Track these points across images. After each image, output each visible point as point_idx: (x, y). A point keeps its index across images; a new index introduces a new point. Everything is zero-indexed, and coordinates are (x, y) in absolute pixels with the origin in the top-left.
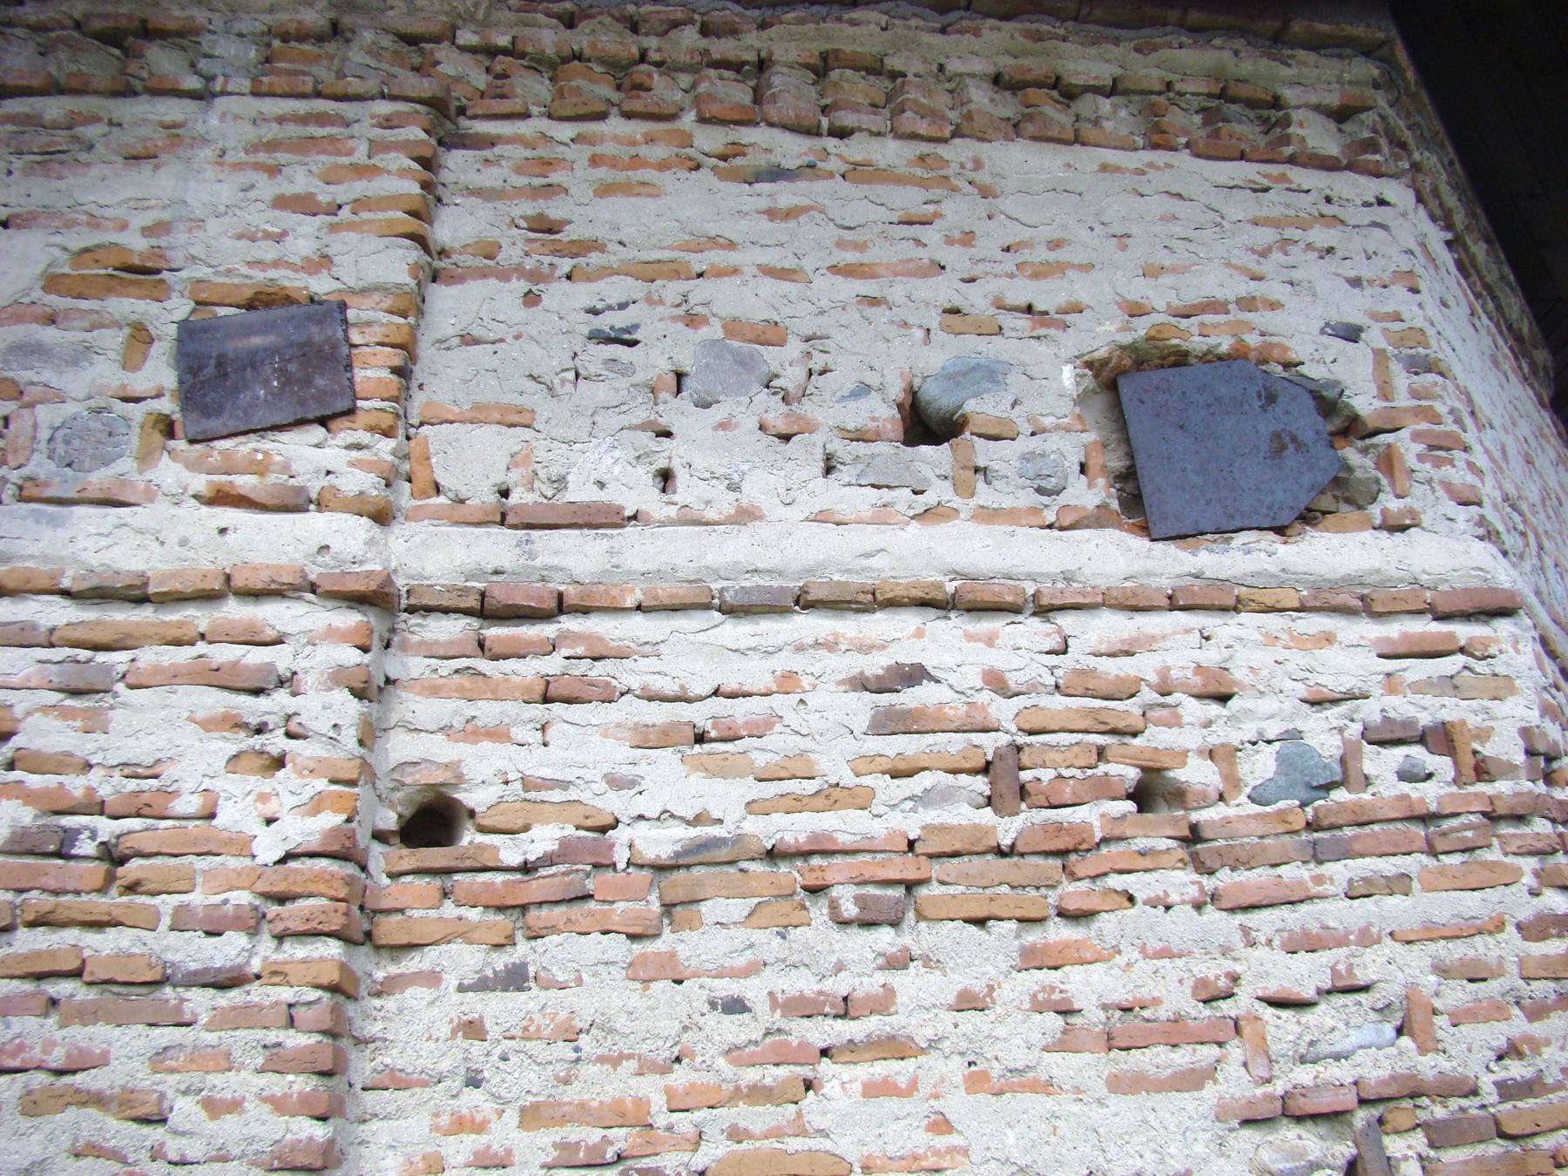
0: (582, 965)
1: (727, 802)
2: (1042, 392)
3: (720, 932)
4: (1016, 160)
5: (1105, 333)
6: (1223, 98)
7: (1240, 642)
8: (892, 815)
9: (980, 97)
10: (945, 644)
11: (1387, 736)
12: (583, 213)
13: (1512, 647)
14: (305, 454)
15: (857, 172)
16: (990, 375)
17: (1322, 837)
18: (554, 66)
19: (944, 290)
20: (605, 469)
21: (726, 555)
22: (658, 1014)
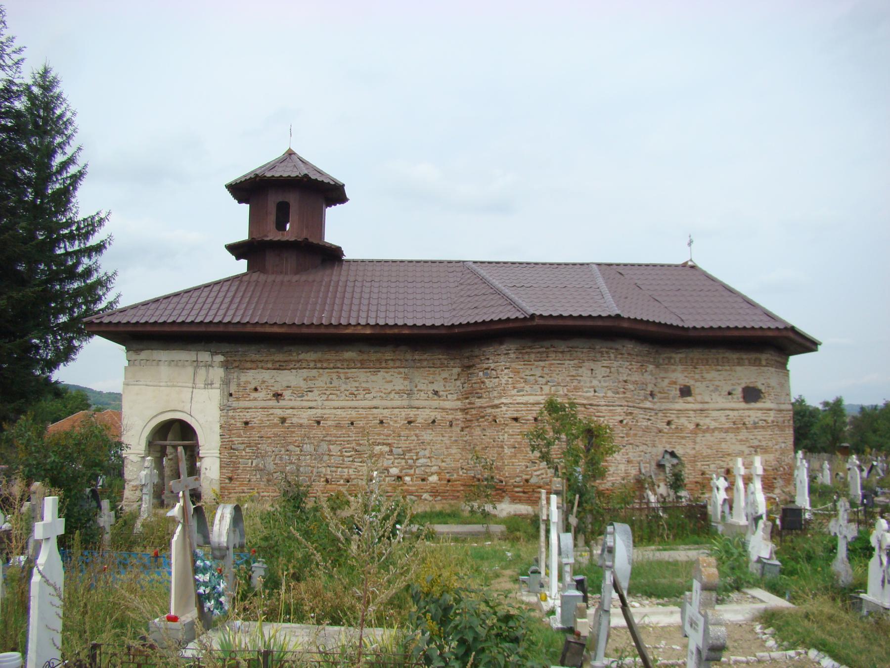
3: (716, 433)
4: (739, 368)
5: (743, 385)
6: (756, 359)
7: (751, 413)
8: (727, 426)
9: (736, 361)
12: (706, 375)
13: (772, 413)
14: (689, 399)
15: (726, 370)
16: (734, 390)
17: (756, 428)
20: (707, 399)
22: (712, 439)
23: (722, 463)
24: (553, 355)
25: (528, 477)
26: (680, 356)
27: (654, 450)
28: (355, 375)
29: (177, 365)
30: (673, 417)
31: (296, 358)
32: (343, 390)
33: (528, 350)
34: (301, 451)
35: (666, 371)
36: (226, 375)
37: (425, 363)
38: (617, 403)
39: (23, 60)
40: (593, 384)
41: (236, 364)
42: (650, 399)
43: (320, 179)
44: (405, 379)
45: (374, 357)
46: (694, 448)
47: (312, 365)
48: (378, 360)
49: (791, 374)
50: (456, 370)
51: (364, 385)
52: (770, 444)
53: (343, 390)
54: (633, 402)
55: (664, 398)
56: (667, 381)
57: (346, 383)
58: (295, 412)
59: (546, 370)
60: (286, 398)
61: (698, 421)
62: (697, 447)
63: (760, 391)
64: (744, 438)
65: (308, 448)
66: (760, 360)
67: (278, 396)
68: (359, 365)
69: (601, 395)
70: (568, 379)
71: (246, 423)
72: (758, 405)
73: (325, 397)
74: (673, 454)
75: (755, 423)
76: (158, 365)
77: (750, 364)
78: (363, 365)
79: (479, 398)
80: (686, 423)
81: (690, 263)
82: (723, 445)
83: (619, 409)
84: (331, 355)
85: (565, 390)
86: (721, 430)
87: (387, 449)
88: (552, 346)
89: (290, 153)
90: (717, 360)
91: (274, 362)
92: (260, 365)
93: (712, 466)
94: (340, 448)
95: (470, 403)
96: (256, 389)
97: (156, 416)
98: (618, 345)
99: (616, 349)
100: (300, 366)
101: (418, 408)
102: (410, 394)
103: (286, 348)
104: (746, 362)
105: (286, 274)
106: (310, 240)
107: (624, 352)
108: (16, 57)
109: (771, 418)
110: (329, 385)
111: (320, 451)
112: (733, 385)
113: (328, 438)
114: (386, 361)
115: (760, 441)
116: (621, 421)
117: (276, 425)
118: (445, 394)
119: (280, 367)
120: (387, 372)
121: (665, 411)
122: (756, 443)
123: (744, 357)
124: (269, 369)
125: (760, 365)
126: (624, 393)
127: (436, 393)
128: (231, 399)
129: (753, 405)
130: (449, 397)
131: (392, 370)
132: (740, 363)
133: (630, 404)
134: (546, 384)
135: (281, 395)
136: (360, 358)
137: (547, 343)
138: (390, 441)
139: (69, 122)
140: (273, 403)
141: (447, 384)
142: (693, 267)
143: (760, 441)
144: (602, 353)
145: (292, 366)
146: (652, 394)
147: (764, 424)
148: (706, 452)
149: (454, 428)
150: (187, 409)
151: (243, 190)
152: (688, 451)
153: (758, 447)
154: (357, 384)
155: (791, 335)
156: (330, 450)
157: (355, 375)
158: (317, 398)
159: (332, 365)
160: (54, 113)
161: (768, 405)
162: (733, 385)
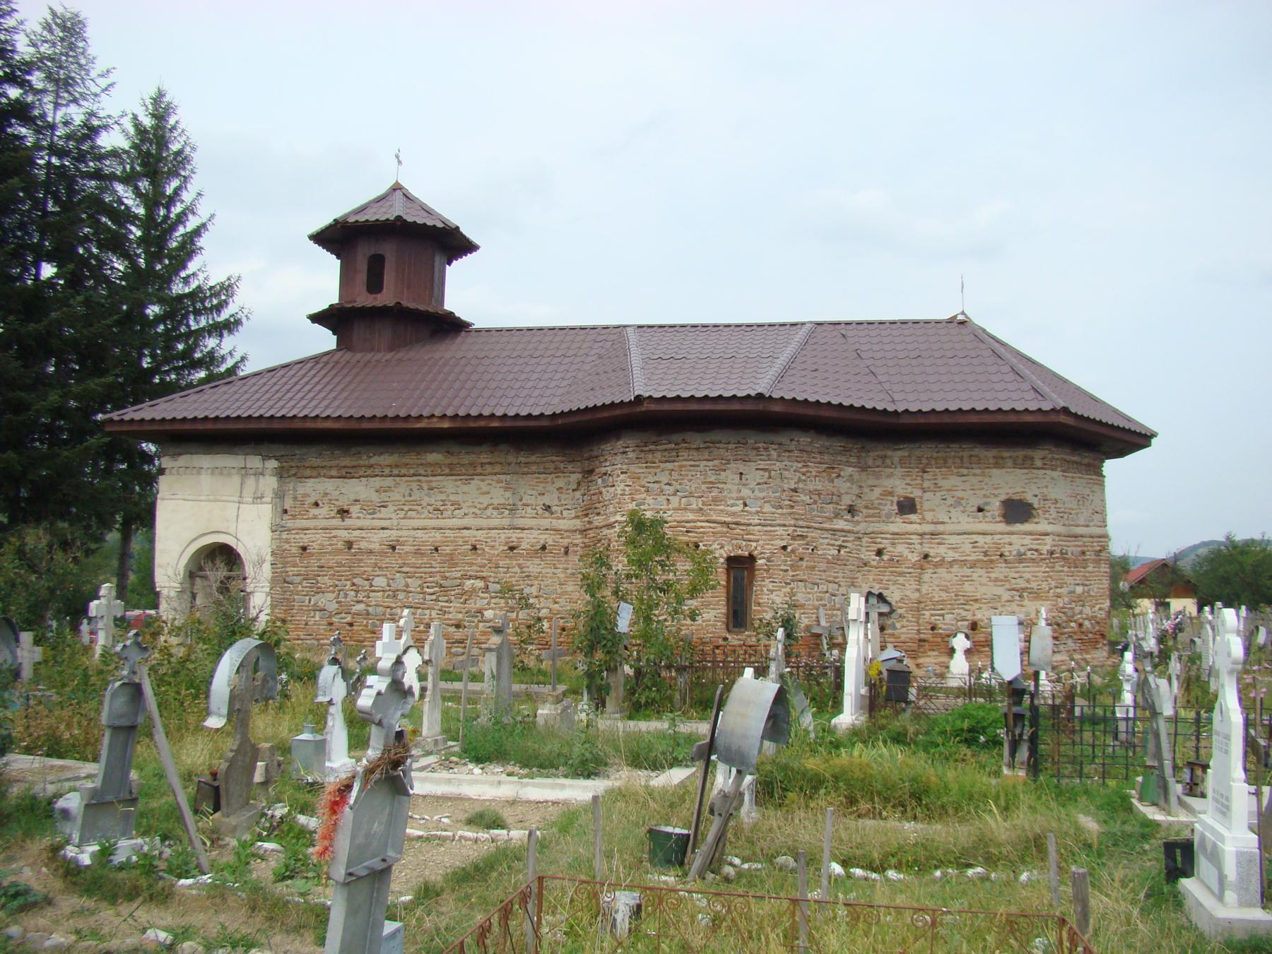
0: (942, 571)
1: (957, 556)
2: (995, 506)
3: (955, 569)
4: (995, 472)
5: (1003, 497)
8: (973, 557)
9: (991, 461)
10: (980, 539)
11: (1030, 550)
12: (941, 482)
13: (1048, 540)
14: (913, 517)
15: (974, 475)
16: (988, 504)
18: (936, 459)
19: (983, 492)
20: (942, 517)
21: (958, 528)
22: (948, 577)
23: (964, 613)
24: (685, 454)
26: (899, 453)
28: (442, 484)
29: (221, 474)
30: (885, 544)
32: (424, 504)
34: (371, 586)
35: (878, 477)
37: (534, 468)
39: (112, 85)
41: (293, 471)
42: (849, 517)
43: (430, 223)
44: (506, 489)
45: (466, 459)
46: (918, 590)
47: (387, 471)
48: (471, 464)
49: (1107, 481)
50: (575, 477)
51: (452, 498)
52: (1044, 585)
53: (424, 504)
54: (812, 520)
55: (873, 516)
56: (877, 491)
58: (363, 534)
60: (354, 515)
61: (926, 549)
62: (924, 589)
63: (1030, 505)
65: (380, 582)
66: (1032, 459)
67: (343, 513)
68: (447, 471)
69: (754, 510)
70: (704, 487)
71: (304, 549)
73: (402, 514)
75: (1020, 554)
76: (199, 473)
78: (452, 471)
79: (598, 514)
80: (906, 553)
81: (960, 317)
82: (967, 587)
83: (780, 530)
84: (411, 458)
86: (963, 563)
87: (480, 584)
88: (684, 441)
89: (397, 188)
90: (961, 458)
91: (340, 468)
92: (323, 472)
93: (948, 617)
95: (590, 522)
96: (317, 504)
98: (784, 438)
100: (371, 472)
101: (523, 529)
102: (513, 510)
103: (353, 450)
104: (1009, 463)
105: (379, 351)
107: (792, 448)
108: (103, 83)
109: (1048, 547)
111: (394, 586)
112: (985, 496)
114: (482, 465)
115: (1028, 581)
116: (784, 548)
117: (339, 552)
118: (559, 509)
119: (347, 475)
121: (872, 535)
123: (1006, 454)
127: (548, 508)
128: (286, 517)
129: (1019, 527)
133: (801, 523)
134: (675, 495)
135: (347, 512)
136: (448, 461)
137: (677, 437)
138: (484, 574)
139: (187, 160)
140: (337, 522)
141: (563, 496)
142: (962, 323)
143: (1028, 581)
144: (757, 449)
145: (361, 473)
146: (851, 510)
147: (1036, 555)
148: (938, 595)
149: (571, 557)
151: (337, 238)
152: (908, 593)
154: (443, 497)
155: (1063, 419)
156: (407, 586)
157: (442, 484)
158: (393, 516)
159: (412, 471)
160: (168, 148)
161: (1043, 526)
162: (985, 496)
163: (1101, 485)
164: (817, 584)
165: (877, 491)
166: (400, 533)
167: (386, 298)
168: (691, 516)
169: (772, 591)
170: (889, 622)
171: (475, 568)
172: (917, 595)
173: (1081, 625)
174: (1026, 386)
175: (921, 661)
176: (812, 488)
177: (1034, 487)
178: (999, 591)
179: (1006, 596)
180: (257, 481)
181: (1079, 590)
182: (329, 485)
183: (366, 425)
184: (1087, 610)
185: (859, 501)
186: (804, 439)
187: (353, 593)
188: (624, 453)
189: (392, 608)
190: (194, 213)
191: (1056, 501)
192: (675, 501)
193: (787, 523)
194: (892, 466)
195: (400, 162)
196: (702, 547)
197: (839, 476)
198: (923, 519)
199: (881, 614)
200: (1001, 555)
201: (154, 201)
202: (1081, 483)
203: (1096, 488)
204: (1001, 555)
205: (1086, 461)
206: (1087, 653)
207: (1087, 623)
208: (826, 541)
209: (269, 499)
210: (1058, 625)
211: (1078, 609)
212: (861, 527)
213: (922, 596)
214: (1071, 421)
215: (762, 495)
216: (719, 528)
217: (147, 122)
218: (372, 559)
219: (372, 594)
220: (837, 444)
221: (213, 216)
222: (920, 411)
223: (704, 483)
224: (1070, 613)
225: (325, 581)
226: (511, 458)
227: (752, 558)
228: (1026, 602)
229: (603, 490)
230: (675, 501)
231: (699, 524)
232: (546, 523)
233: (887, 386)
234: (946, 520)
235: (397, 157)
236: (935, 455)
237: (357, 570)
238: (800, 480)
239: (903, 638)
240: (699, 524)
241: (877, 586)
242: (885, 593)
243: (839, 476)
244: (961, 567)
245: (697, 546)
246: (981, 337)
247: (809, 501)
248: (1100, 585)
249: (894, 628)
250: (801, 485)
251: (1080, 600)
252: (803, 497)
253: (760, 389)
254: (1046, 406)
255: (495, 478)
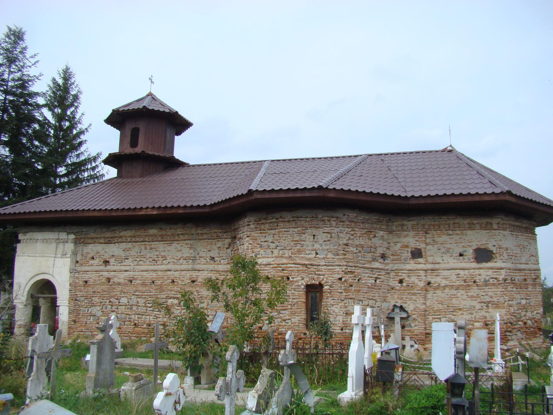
0: (439, 292)
2: (470, 253)
3: (447, 290)
4: (469, 232)
5: (475, 247)
7: (482, 271)
8: (458, 283)
9: (467, 226)
10: (461, 272)
11: (492, 278)
12: (437, 239)
13: (503, 272)
14: (420, 260)
15: (457, 234)
16: (465, 251)
17: (486, 285)
18: (434, 225)
19: (462, 244)
20: (439, 260)
22: (443, 295)
24: (281, 224)
25: (261, 325)
27: (385, 305)
28: (157, 246)
29: (47, 242)
30: (404, 276)
31: (118, 235)
33: (264, 221)
36: (75, 248)
37: (205, 236)
38: (336, 263)
40: (314, 248)
42: (382, 261)
44: (191, 248)
45: (169, 232)
46: (424, 304)
47: (129, 239)
50: (228, 241)
51: (162, 254)
52: (502, 300)
54: (357, 262)
56: (399, 245)
57: (150, 252)
58: (116, 274)
59: (276, 237)
60: (111, 264)
61: (429, 279)
62: (428, 303)
63: (491, 252)
64: (475, 294)
65: (124, 300)
66: (491, 224)
68: (160, 239)
69: (322, 256)
70: (292, 243)
71: (86, 282)
72: (489, 264)
73: (136, 263)
74: (402, 308)
75: (486, 281)
76: (36, 242)
77: (481, 228)
78: (163, 239)
80: (416, 281)
81: (449, 148)
82: (454, 301)
83: (338, 269)
84: (141, 232)
85: (290, 253)
86: (452, 287)
89: (150, 94)
92: (97, 240)
94: (144, 300)
96: (93, 258)
97: (33, 277)
98: (339, 214)
99: (337, 218)
101: (199, 271)
102: (194, 259)
103: (112, 229)
104: (478, 226)
106: (147, 152)
107: (344, 219)
108: (33, 61)
109: (503, 276)
110: (139, 254)
113: (137, 293)
115: (491, 297)
117: (103, 284)
120: (178, 244)
122: (488, 299)
123: (475, 222)
124: (101, 243)
125: (492, 229)
126: (345, 255)
128: (77, 265)
129: (484, 265)
130: (222, 261)
131: (182, 242)
132: (471, 227)
133: (350, 264)
134: (276, 248)
135: (108, 262)
136: (160, 233)
137: (277, 215)
140: (102, 267)
141: (221, 252)
142: (450, 151)
143: (491, 297)
144: (324, 220)
145: (116, 241)
146: (383, 256)
148: (437, 307)
150: (51, 272)
152: (418, 305)
153: (489, 302)
154: (157, 253)
155: (508, 198)
156: (138, 302)
158: (131, 264)
159: (142, 239)
161: (499, 264)
163: (535, 240)
164: (362, 301)
165: (399, 245)
166: (135, 273)
167: (138, 150)
168: (285, 261)
169: (333, 305)
170: (407, 323)
171: (173, 292)
172: (424, 306)
173: (525, 323)
174: (486, 181)
175: (427, 346)
176: (357, 243)
177: (492, 240)
178: (474, 303)
179: (478, 306)
180: (64, 246)
181: (523, 302)
182: (98, 248)
183: (114, 214)
184: (529, 314)
185: (388, 251)
186: (352, 215)
187: (110, 306)
188: (248, 225)
189: (130, 315)
190: (80, 123)
191: (507, 249)
192: (276, 252)
193: (341, 264)
194: (408, 230)
195: (152, 82)
196: (291, 279)
197: (375, 236)
198: (427, 261)
199: (402, 318)
200: (474, 282)
201: (60, 118)
202: (522, 239)
203: (531, 241)
204: (474, 282)
205: (524, 225)
206: (530, 340)
207: (529, 322)
208: (367, 275)
209: (69, 256)
210: (511, 323)
211: (523, 314)
212: (389, 267)
213: (427, 307)
214: (514, 200)
215: (327, 248)
216: (301, 268)
217: (60, 82)
218: (120, 288)
219: (119, 307)
220: (374, 217)
221: (90, 125)
222: (421, 196)
223: (292, 241)
224: (518, 316)
225: (96, 300)
226: (193, 231)
227: (321, 286)
228: (490, 310)
229: (239, 247)
230: (276, 252)
231: (289, 265)
232: (211, 267)
233: (403, 184)
234: (441, 261)
235: (151, 79)
236: (433, 223)
237: (112, 294)
238: (349, 239)
239: (416, 332)
240: (289, 265)
241: (400, 301)
242: (404, 306)
243: (375, 236)
244: (450, 289)
245: (288, 278)
246: (460, 157)
247: (355, 251)
248: (537, 299)
249: (411, 326)
250: (350, 242)
251: (524, 308)
252: (352, 249)
253: (323, 184)
254: (497, 191)
255: (185, 242)
